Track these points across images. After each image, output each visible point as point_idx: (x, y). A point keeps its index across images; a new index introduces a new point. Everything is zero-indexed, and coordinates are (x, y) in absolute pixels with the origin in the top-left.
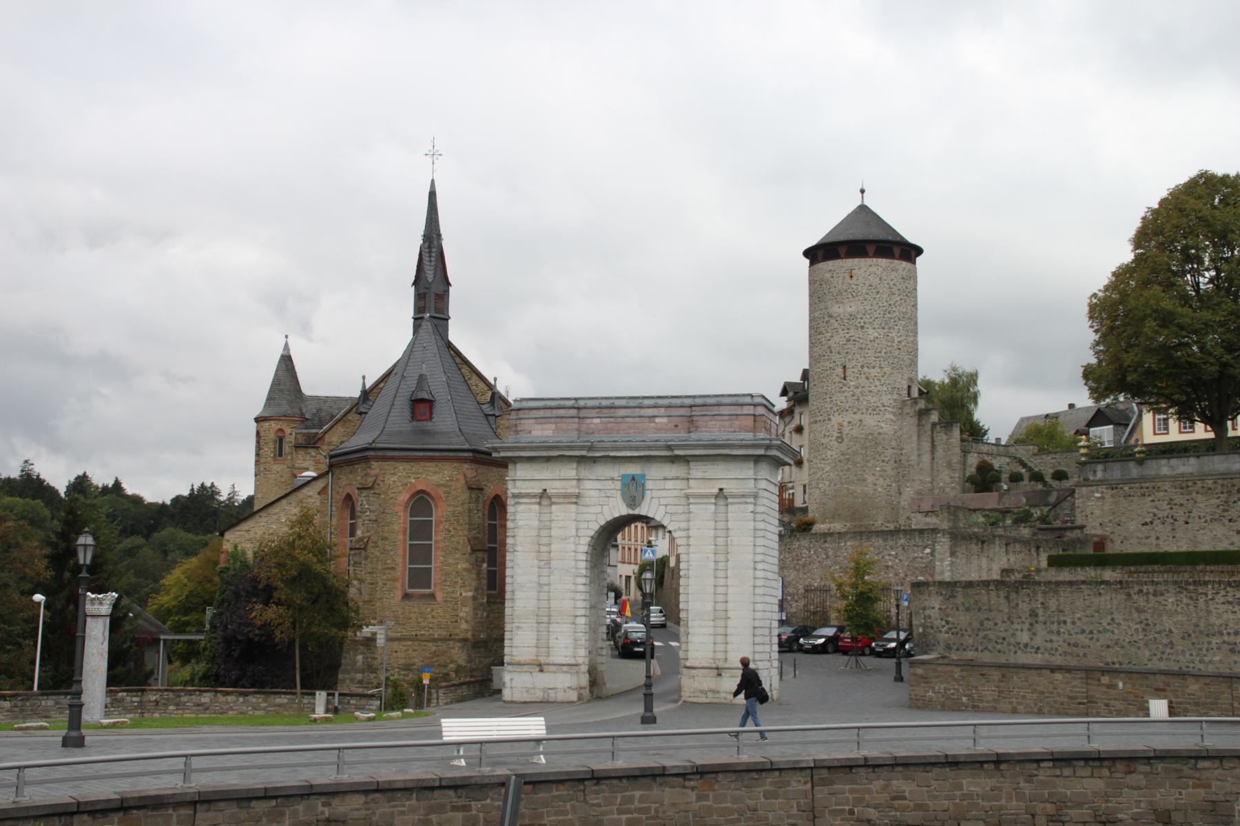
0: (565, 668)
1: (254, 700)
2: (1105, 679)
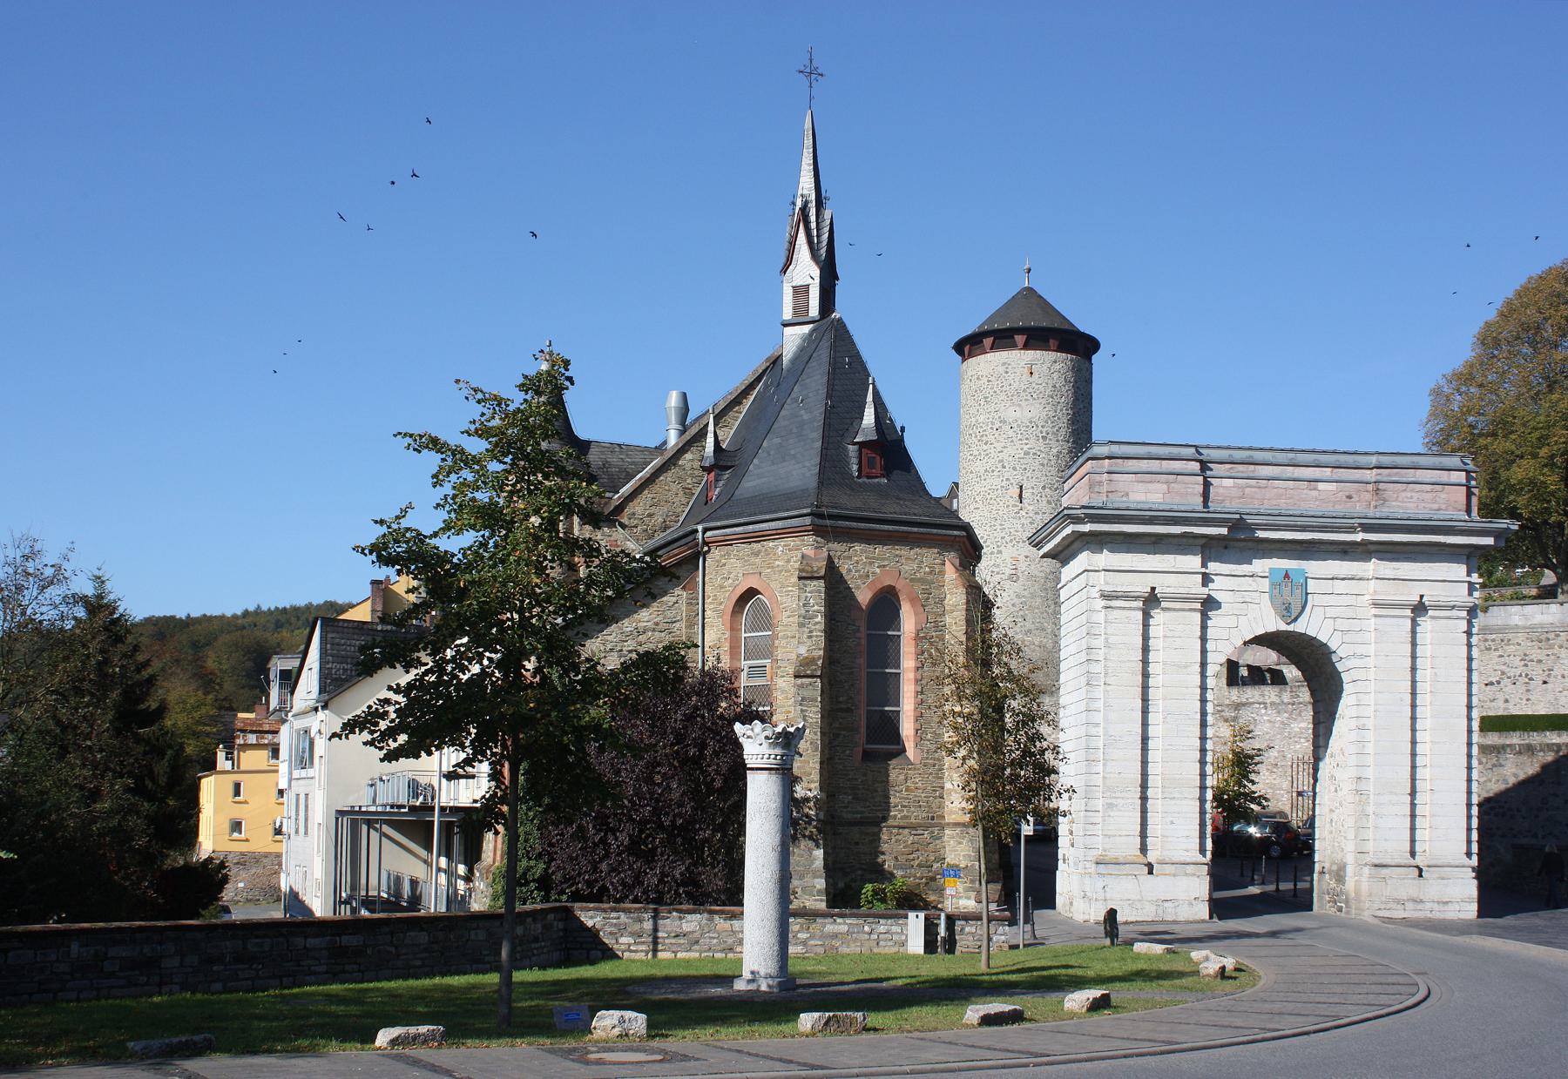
0: (1190, 869)
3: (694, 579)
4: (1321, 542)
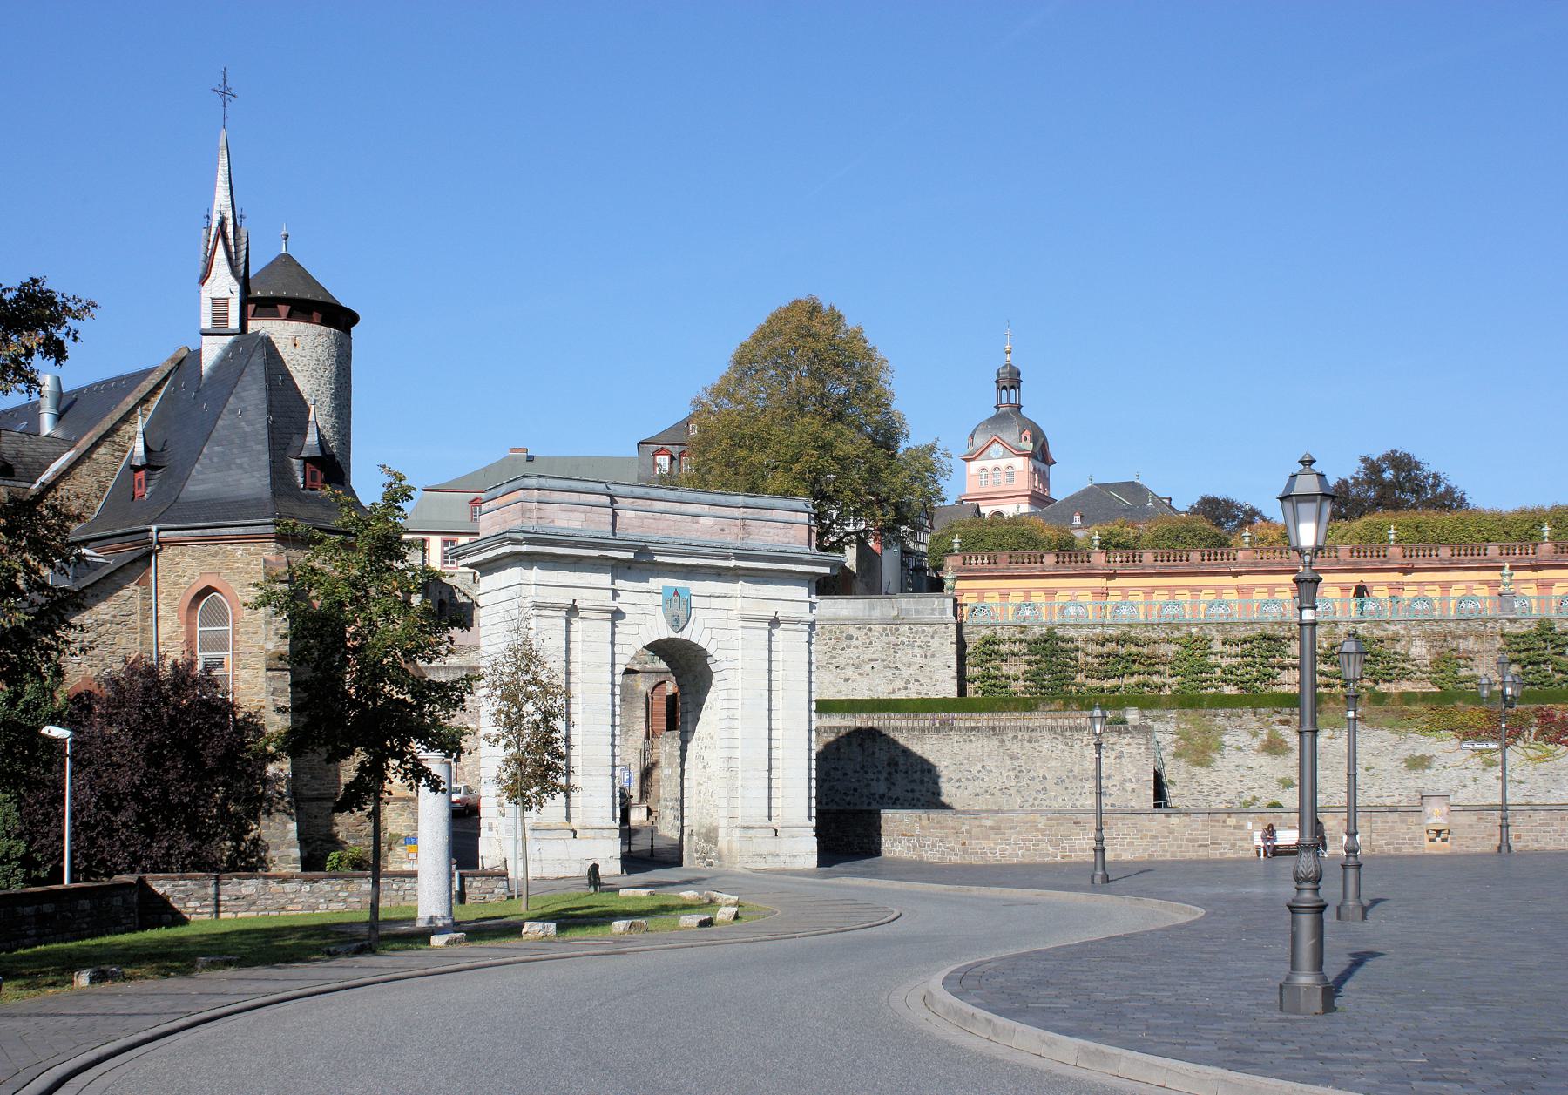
0: (606, 833)
1: (327, 888)
2: (1232, 821)
3: (147, 576)
4: (702, 566)
